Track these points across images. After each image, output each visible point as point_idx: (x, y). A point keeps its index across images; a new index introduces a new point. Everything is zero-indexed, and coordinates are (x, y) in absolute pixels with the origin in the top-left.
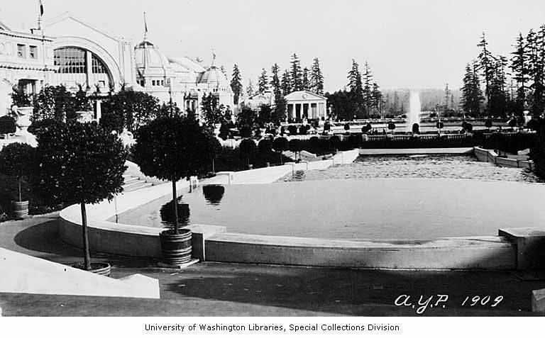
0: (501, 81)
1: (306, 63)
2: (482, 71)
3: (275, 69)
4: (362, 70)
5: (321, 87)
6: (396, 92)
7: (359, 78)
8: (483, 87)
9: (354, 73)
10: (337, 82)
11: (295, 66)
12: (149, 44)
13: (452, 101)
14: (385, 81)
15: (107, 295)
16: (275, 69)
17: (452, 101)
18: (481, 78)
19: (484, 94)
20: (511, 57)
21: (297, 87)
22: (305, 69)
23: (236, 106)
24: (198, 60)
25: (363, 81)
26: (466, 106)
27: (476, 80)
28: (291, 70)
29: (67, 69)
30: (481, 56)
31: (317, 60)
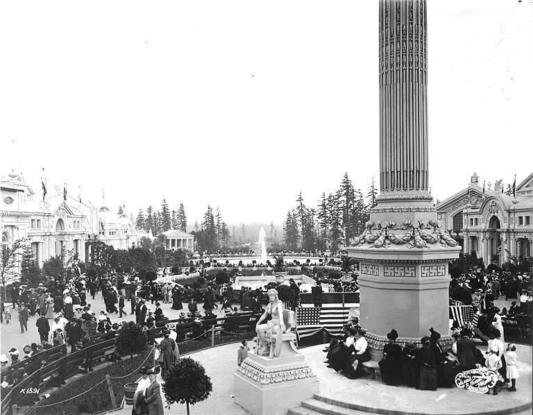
0: (310, 226)
1: (173, 207)
2: (299, 218)
3: (150, 209)
4: (215, 214)
5: (184, 224)
6: (243, 225)
7: (212, 217)
8: (300, 229)
9: (209, 216)
10: (195, 219)
11: (164, 208)
12: (107, 209)
13: (276, 235)
14: (231, 219)
15: (429, 71)
16: (150, 209)
17: (276, 235)
18: (299, 223)
19: (300, 234)
20: (318, 210)
21: (309, 311)
22: (173, 212)
23: (154, 238)
24: (121, 211)
25: (215, 221)
26: (288, 241)
27: (294, 223)
28: (161, 211)
29: (173, 245)
30: (299, 207)
31: (182, 205)
